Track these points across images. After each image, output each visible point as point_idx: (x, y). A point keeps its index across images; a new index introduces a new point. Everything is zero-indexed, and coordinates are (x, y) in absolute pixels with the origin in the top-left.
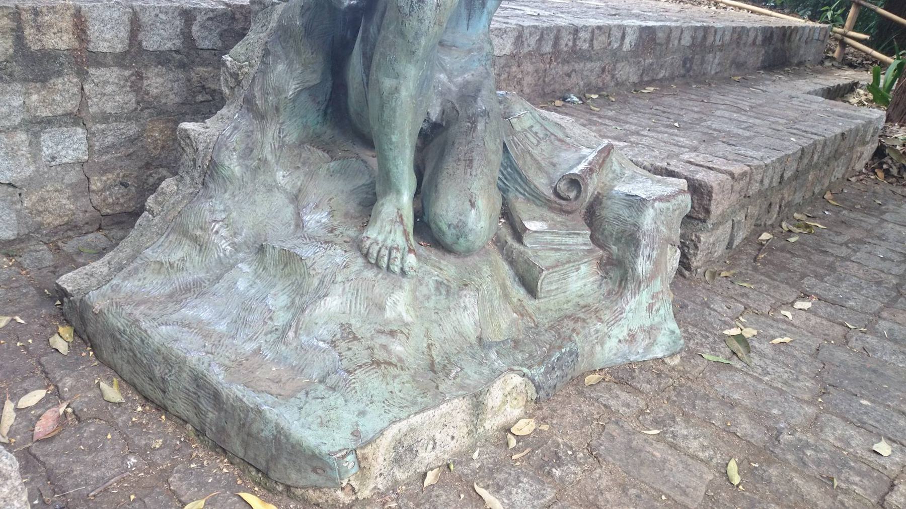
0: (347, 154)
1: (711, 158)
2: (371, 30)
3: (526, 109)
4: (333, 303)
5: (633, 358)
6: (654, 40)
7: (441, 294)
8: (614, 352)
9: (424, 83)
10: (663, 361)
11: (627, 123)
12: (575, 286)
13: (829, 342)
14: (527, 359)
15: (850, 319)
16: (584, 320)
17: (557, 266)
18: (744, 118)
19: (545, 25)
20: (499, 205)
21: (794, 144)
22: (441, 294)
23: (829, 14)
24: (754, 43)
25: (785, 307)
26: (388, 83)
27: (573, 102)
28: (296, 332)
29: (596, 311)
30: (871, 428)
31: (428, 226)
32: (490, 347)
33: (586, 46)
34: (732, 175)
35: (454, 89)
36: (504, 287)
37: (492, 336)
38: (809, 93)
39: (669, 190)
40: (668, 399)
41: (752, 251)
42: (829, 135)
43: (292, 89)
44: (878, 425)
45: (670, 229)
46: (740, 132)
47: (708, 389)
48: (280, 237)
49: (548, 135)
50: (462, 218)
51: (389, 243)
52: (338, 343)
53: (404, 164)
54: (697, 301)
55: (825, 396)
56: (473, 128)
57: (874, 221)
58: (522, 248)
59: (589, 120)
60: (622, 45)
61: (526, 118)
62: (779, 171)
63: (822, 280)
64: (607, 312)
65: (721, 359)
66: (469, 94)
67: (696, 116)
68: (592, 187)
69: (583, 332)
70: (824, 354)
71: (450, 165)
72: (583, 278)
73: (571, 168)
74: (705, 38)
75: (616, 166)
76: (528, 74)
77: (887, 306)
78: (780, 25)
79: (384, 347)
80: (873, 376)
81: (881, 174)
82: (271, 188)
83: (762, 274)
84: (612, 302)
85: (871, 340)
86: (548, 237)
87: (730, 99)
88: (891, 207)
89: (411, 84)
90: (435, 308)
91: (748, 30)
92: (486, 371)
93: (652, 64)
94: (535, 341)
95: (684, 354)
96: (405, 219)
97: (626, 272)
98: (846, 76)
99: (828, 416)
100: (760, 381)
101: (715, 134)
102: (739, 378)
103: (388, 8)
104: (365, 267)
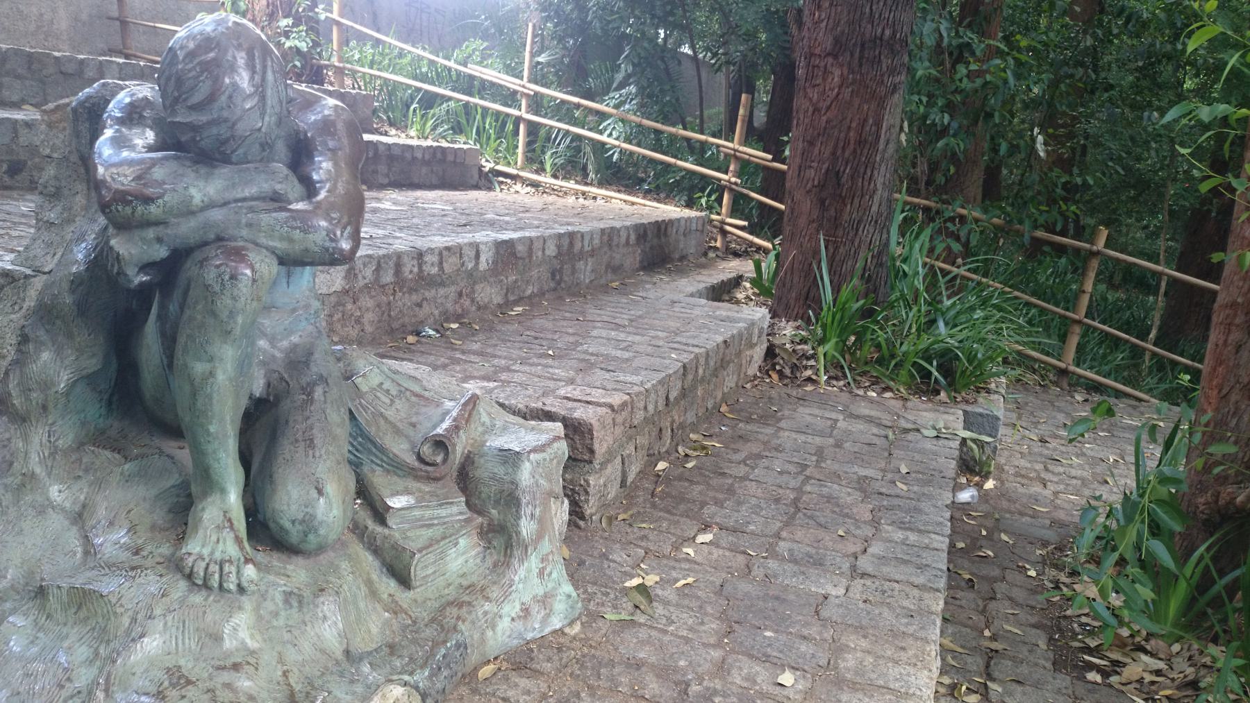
0: (144, 450)
1: (588, 390)
2: (171, 307)
3: (371, 364)
4: (152, 645)
5: (529, 636)
6: (514, 254)
7: (291, 607)
8: (508, 633)
9: (243, 366)
10: (563, 633)
11: (495, 356)
12: (455, 564)
13: (733, 575)
14: (407, 665)
15: (752, 547)
16: (469, 604)
17: (431, 545)
18: (622, 336)
19: (381, 252)
20: (352, 486)
21: (674, 361)
22: (291, 607)
23: (703, 201)
24: (627, 243)
25: (686, 544)
26: (199, 368)
27: (430, 336)
28: (106, 691)
29: (483, 590)
30: (775, 660)
31: (265, 526)
32: (361, 659)
33: (435, 270)
34: (611, 407)
35: (278, 355)
36: (369, 583)
37: (362, 645)
38: (692, 295)
39: (544, 438)
40: (571, 675)
41: (648, 485)
42: (711, 345)
43: (63, 379)
44: (781, 655)
45: (550, 481)
46: (619, 353)
47: (613, 653)
48: (63, 569)
49: (402, 392)
50: (308, 510)
51: (218, 556)
52: (167, 693)
53: (228, 456)
54: (595, 554)
55: (732, 635)
56: (310, 400)
57: (769, 430)
58: (386, 531)
59: (450, 358)
60: (477, 264)
61: (373, 375)
62: (662, 393)
63: (722, 507)
64: (494, 588)
65: (624, 616)
66: (299, 360)
67: (571, 339)
68: (460, 447)
69: (470, 618)
70: (728, 588)
71: (286, 448)
72: (464, 553)
73: (435, 427)
74: (571, 244)
75: (485, 418)
76: (368, 309)
77: (787, 524)
78: (652, 220)
79: (228, 686)
80: (776, 603)
81: (775, 376)
82: (43, 509)
83: (661, 510)
84: (499, 575)
85: (772, 564)
86: (417, 513)
87: (606, 314)
88: (786, 413)
89: (229, 366)
90: (287, 626)
91: (619, 230)
92: (359, 689)
93: (516, 281)
94: (414, 641)
95: (584, 619)
96: (235, 523)
97: (510, 538)
98: (733, 267)
99: (734, 656)
100: (665, 632)
101: (593, 359)
102: (643, 633)
103: (193, 285)
104: (190, 591)
